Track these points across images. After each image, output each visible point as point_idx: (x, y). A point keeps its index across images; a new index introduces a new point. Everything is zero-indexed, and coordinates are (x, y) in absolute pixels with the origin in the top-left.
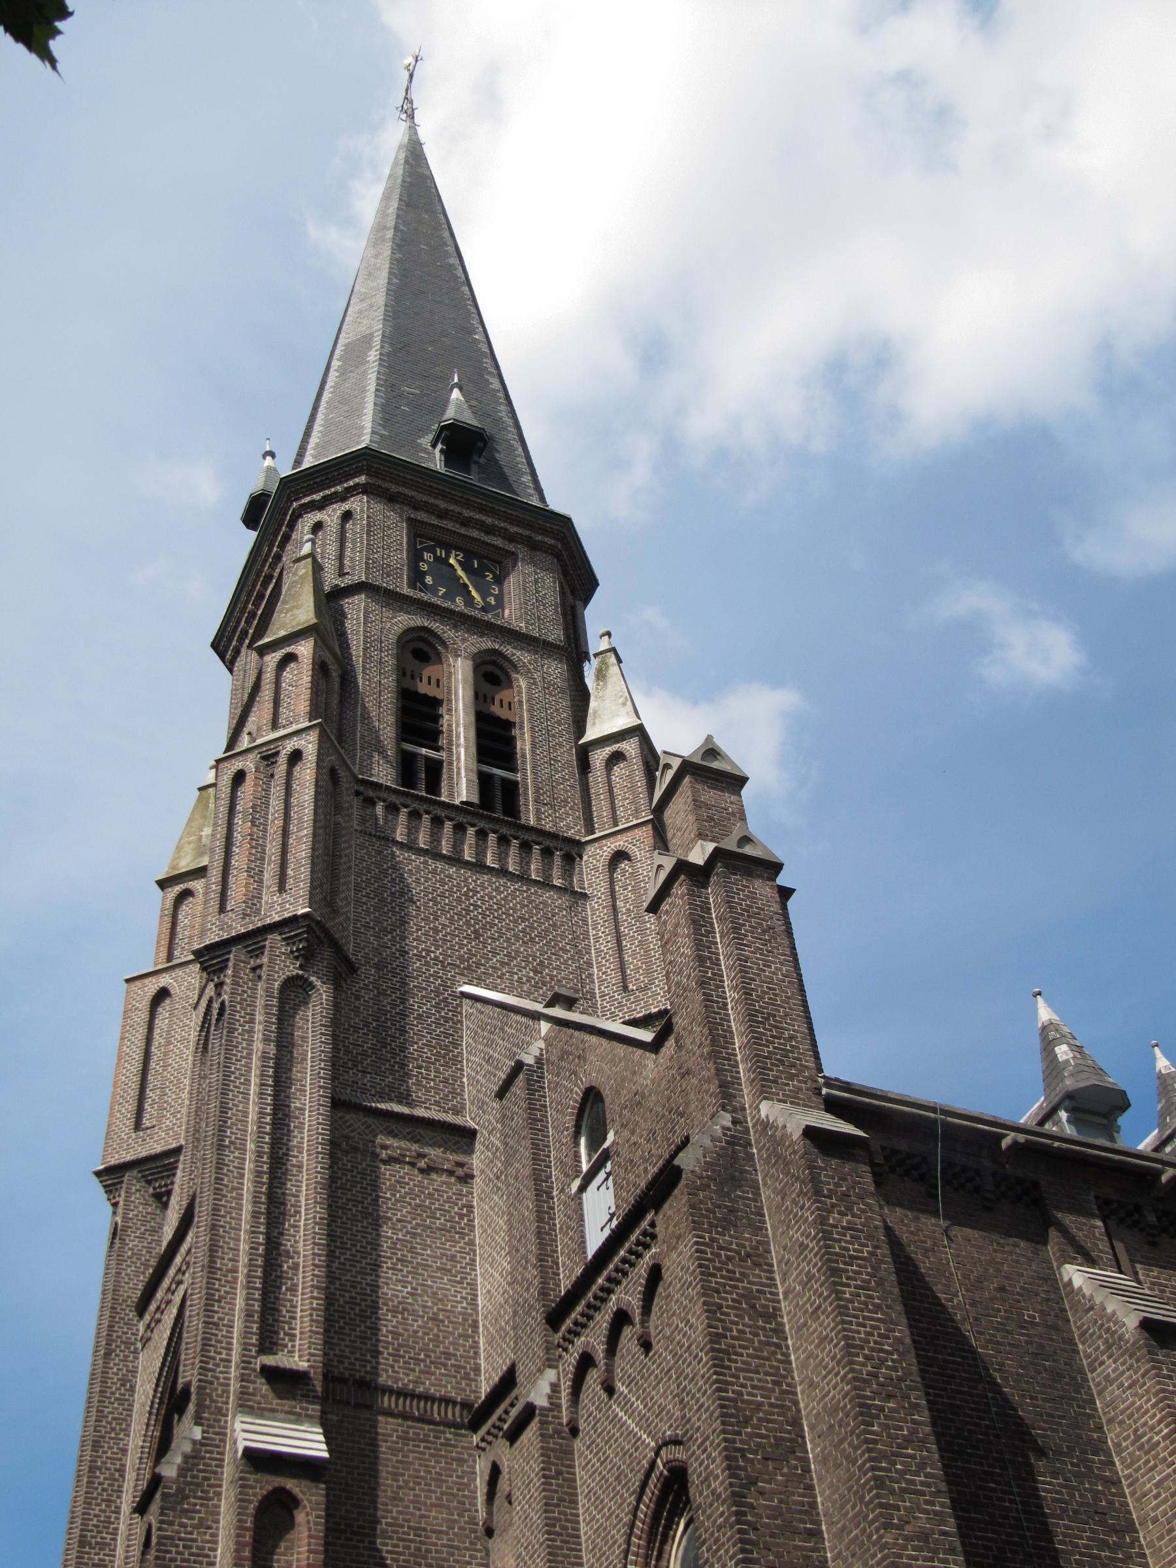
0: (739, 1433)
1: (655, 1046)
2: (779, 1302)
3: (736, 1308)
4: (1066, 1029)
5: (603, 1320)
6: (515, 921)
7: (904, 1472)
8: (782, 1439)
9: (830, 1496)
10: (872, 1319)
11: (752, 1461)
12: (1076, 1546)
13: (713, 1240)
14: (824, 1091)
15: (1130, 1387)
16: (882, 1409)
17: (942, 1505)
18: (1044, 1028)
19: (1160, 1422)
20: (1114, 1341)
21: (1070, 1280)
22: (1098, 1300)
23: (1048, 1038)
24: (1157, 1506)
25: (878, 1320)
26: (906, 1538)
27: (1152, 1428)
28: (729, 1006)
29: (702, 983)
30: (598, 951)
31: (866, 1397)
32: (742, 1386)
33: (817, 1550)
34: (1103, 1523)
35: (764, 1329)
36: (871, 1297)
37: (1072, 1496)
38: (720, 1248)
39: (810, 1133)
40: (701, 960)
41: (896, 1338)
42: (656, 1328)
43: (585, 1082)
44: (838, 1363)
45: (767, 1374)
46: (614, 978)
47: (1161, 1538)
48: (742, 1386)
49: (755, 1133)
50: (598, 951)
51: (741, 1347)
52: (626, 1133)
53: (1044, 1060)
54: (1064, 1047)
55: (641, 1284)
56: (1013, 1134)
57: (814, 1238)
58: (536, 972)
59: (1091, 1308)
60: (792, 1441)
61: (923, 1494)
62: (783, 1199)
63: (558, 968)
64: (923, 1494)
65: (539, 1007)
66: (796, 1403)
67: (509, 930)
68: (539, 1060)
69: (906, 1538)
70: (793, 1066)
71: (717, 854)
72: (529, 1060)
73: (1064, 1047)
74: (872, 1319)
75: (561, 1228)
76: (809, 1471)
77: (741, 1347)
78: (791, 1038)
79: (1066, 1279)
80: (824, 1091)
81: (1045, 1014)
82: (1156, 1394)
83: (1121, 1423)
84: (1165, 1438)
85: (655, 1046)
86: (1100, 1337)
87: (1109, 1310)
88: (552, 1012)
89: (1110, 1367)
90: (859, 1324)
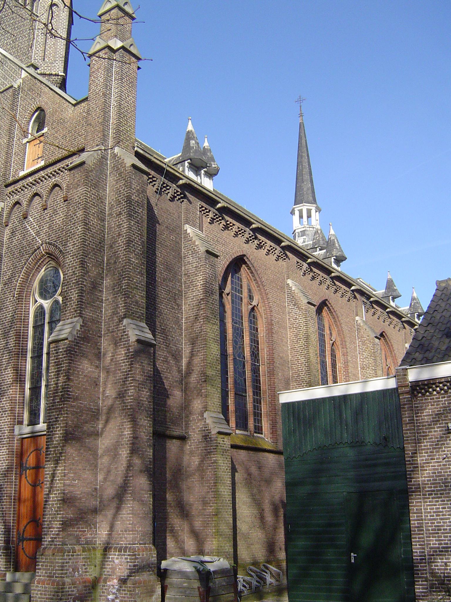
0: (87, 257)
1: (75, 105)
2: (105, 216)
3: (93, 216)
4: (195, 136)
5: (29, 193)
6: (10, 19)
7: (136, 282)
8: (98, 261)
9: (109, 282)
10: (137, 233)
11: (88, 266)
12: (167, 307)
13: (91, 190)
14: (136, 149)
15: (195, 267)
16: (134, 262)
17: (144, 294)
18: (188, 132)
19: (201, 280)
20: (194, 252)
21: (186, 230)
22: (194, 239)
23: (189, 136)
24: (191, 302)
25: (139, 234)
26: (132, 302)
27: (198, 281)
28: (112, 107)
29: (104, 95)
30: (37, 41)
31: (131, 258)
32: (91, 242)
33: (101, 296)
34: (175, 303)
35: (100, 224)
36: (139, 226)
37: (169, 293)
38: (92, 194)
39: (134, 166)
40: (107, 86)
41: (142, 241)
42: (51, 205)
43: (39, 104)
44: (124, 244)
45: (98, 239)
46: (41, 54)
47: (189, 310)
48: (91, 242)
49: (111, 156)
50: (37, 41)
51: (93, 229)
52: (53, 131)
53: (185, 143)
54: (194, 142)
55: (49, 188)
56: (186, 180)
57: (126, 202)
58: (13, 42)
59: (191, 240)
60: (101, 262)
61: (139, 289)
62: (116, 183)
63: (21, 43)
64: (139, 289)
65: (24, 66)
66: (104, 250)
67: (7, 21)
68: (19, 87)
69: (132, 302)
70: (128, 136)
71: (123, 48)
72: (16, 86)
73: (194, 142)
74: (137, 233)
75: (15, 153)
76: (104, 272)
77: (93, 229)
78: (130, 126)
79: (185, 229)
80: (136, 149)
81: (190, 127)
82: (203, 272)
83: (189, 276)
84: (201, 285)
85: (75, 105)
86: (191, 250)
87: (197, 244)
88: (27, 69)
89: (191, 259)
90: (133, 234)
